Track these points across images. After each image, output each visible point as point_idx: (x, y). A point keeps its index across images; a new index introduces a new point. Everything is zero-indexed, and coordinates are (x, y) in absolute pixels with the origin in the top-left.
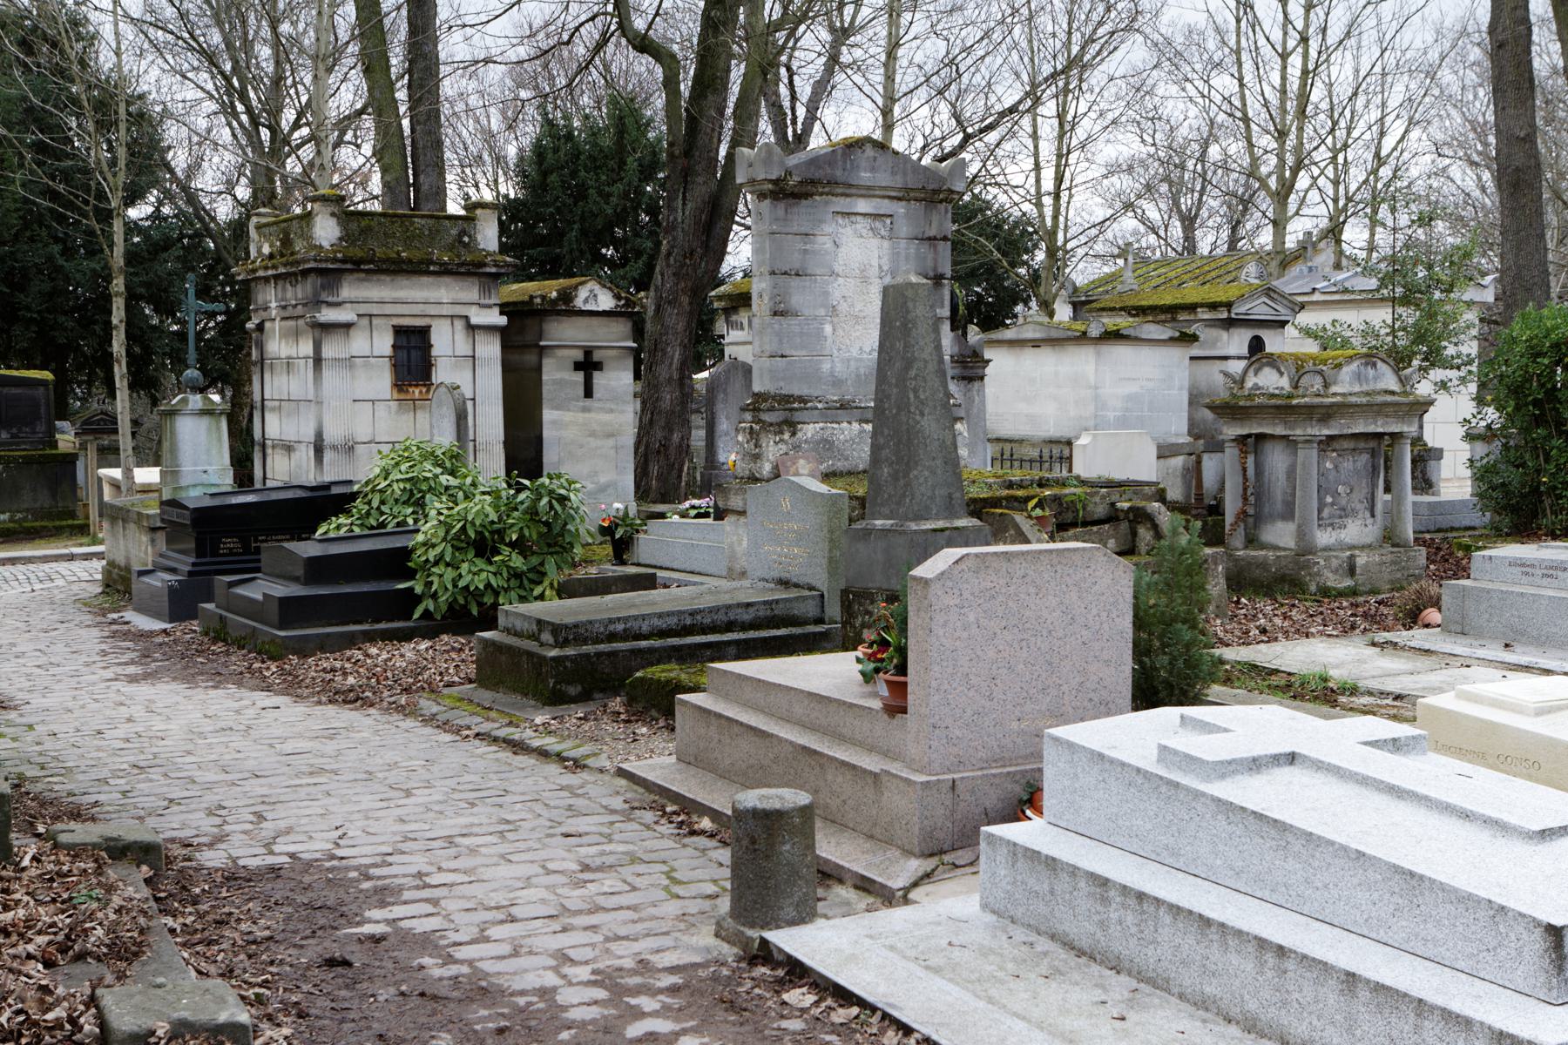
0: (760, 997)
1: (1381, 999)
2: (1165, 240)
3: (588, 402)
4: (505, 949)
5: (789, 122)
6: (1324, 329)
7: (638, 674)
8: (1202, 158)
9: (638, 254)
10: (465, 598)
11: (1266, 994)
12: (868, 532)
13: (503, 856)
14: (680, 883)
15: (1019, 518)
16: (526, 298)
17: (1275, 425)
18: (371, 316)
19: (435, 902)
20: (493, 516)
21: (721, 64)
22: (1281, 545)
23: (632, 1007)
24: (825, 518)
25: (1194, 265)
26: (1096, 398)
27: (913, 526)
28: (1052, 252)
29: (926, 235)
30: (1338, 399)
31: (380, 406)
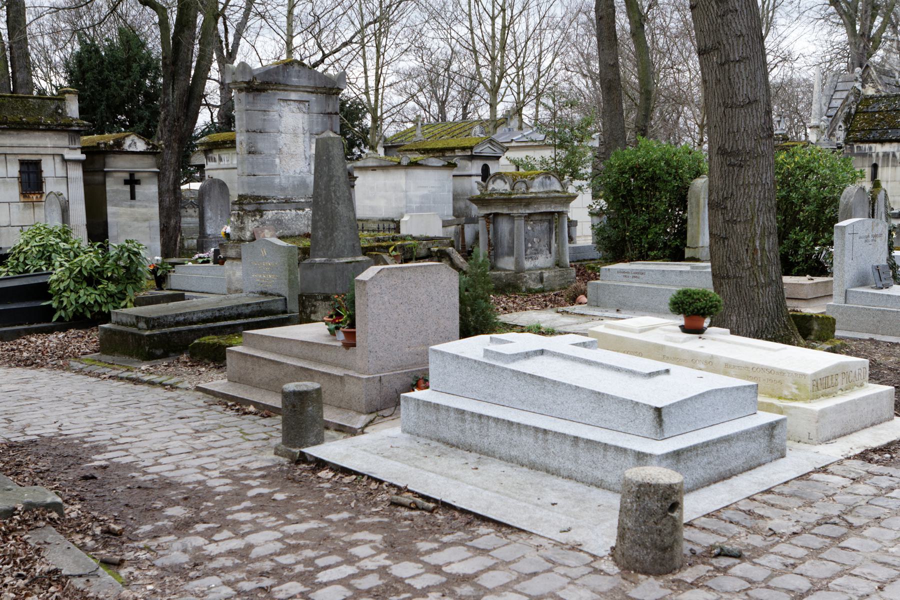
0: (306, 476)
1: (589, 446)
2: (429, 112)
3: (133, 202)
4: (173, 467)
5: (224, 46)
6: (522, 160)
7: (196, 341)
8: (447, 70)
9: (141, 119)
10: (83, 309)
11: (539, 451)
12: (312, 265)
13: (151, 429)
14: (247, 434)
15: (385, 256)
16: (95, 144)
17: (503, 208)
18: (5, 154)
19: (127, 450)
20: (97, 263)
21: (192, 13)
22: (507, 268)
23: (246, 485)
24: (286, 259)
25: (447, 127)
26: (406, 197)
27: (336, 261)
28: (375, 119)
29: (327, 112)
30: (533, 195)
31: (13, 206)
